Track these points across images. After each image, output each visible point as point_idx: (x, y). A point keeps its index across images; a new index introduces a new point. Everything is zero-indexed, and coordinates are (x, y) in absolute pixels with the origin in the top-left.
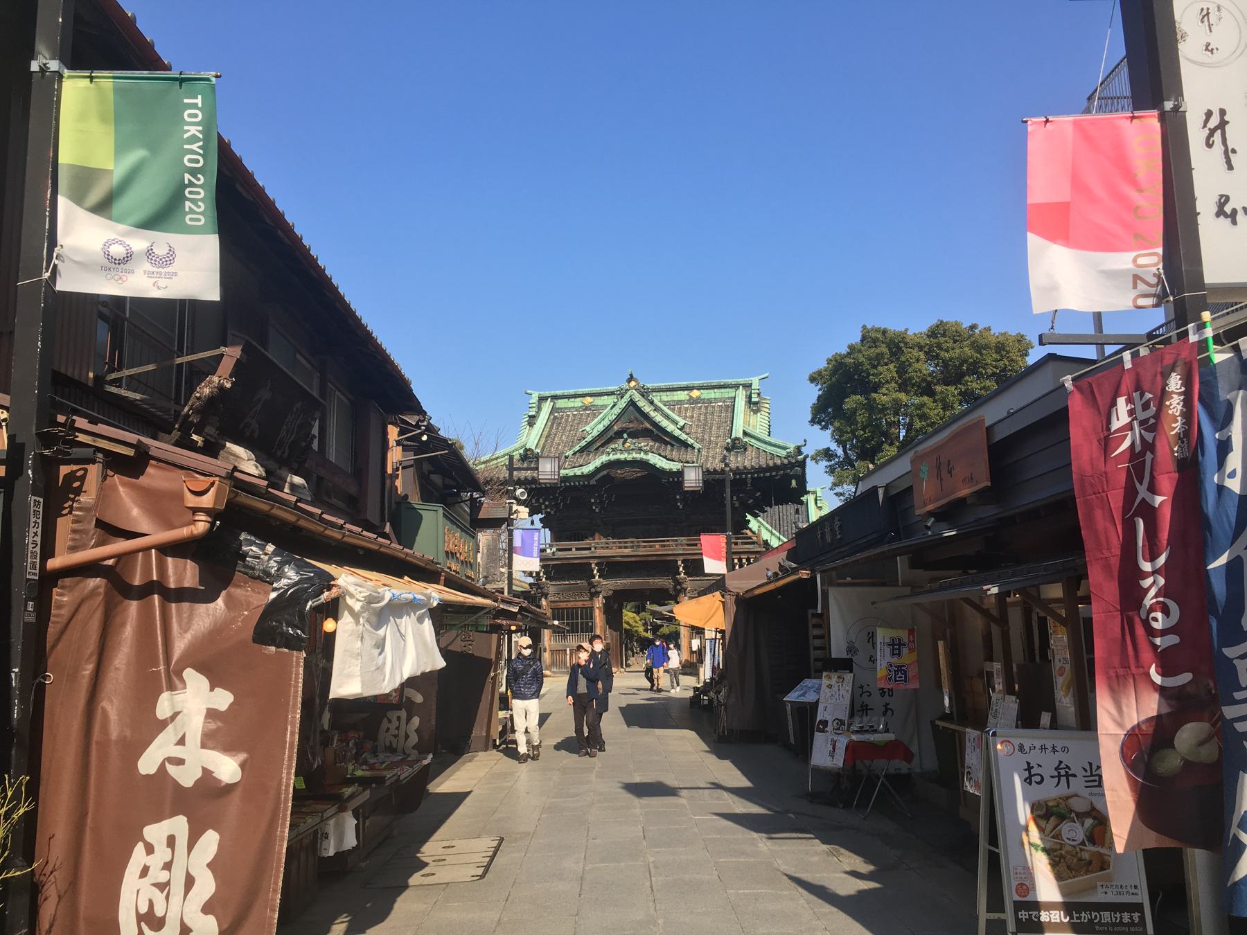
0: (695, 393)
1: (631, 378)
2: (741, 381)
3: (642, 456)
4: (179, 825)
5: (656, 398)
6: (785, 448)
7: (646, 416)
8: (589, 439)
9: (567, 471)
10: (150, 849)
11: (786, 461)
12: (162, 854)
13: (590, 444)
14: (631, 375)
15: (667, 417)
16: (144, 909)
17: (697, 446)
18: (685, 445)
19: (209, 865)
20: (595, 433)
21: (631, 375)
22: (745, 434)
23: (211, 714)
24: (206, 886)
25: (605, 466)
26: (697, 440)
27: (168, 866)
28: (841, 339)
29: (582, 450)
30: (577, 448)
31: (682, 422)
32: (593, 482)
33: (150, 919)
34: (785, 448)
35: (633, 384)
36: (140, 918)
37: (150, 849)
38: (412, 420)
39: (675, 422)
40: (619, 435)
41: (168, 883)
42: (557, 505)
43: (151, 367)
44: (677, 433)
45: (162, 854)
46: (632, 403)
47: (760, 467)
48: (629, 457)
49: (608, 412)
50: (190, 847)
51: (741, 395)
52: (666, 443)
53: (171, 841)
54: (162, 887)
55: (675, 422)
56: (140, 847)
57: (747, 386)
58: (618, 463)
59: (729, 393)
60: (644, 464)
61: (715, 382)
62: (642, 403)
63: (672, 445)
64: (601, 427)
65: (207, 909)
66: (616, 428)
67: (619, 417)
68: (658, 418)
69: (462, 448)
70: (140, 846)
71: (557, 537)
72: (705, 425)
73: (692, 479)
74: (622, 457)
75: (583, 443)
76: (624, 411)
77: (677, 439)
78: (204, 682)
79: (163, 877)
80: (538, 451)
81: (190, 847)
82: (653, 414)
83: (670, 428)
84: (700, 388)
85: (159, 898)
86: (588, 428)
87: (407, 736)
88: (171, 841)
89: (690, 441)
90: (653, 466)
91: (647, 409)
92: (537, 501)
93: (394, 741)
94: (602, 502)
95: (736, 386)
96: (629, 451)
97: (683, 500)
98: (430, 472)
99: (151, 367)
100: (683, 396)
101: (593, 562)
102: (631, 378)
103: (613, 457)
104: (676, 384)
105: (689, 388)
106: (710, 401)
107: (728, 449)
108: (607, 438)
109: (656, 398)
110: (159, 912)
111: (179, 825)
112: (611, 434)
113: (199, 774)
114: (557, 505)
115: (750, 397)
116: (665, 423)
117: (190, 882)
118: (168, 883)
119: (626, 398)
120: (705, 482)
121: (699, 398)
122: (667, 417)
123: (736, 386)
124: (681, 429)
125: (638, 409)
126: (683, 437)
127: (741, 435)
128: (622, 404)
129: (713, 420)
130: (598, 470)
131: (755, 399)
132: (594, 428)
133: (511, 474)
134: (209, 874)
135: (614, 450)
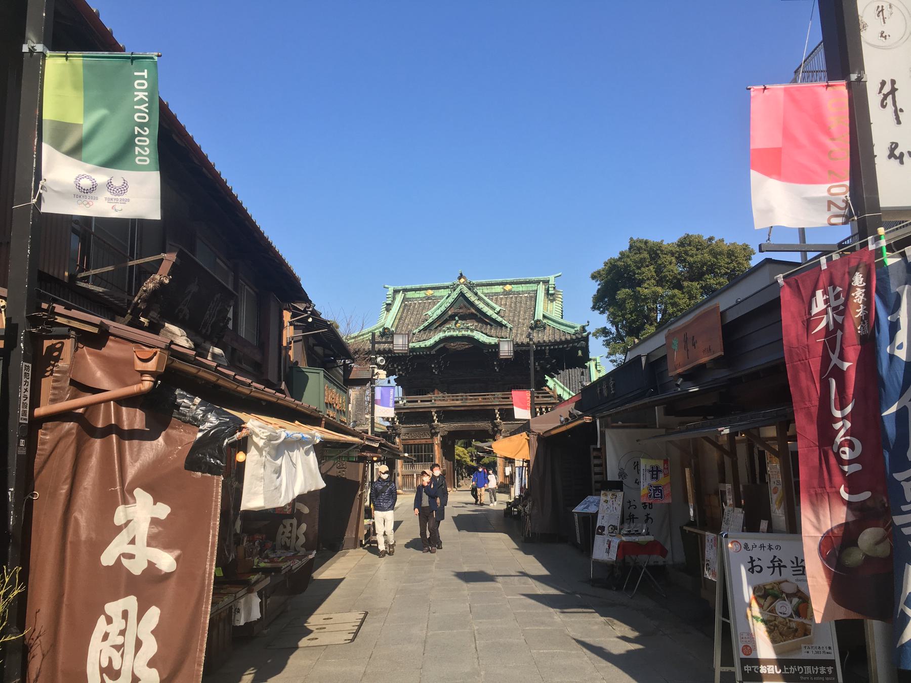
0: (508, 287)
1: (461, 276)
2: (542, 278)
3: (469, 333)
4: (131, 603)
5: (479, 291)
6: (573, 327)
7: (472, 304)
8: (430, 320)
9: (414, 344)
10: (109, 620)
11: (574, 337)
12: (119, 624)
13: (431, 324)
14: (461, 274)
15: (488, 305)
16: (105, 664)
17: (509, 326)
18: (500, 325)
19: (153, 632)
20: (435, 316)
21: (461, 274)
22: (544, 317)
23: (154, 521)
24: (151, 647)
25: (442, 340)
26: (509, 321)
27: (122, 633)
28: (614, 248)
29: (425, 329)
30: (422, 327)
31: (498, 308)
32: (433, 352)
33: (110, 671)
34: (573, 327)
35: (462, 280)
36: (102, 670)
37: (109, 620)
38: (301, 307)
39: (493, 309)
40: (452, 317)
41: (123, 645)
42: (407, 369)
44: (495, 316)
45: (119, 624)
46: (462, 294)
47: (556, 341)
48: (460, 334)
49: (444, 301)
50: (139, 619)
51: (541, 289)
52: (487, 324)
53: (125, 615)
54: (118, 648)
55: (493, 309)
56: (102, 619)
57: (546, 282)
58: (451, 339)
59: (533, 287)
60: (470, 339)
61: (522, 279)
62: (469, 295)
63: (491, 325)
64: (439, 312)
65: (151, 664)
66: (450, 313)
67: (452, 305)
68: (481, 305)
70: (102, 618)
71: (407, 392)
72: (515, 310)
73: (506, 350)
74: (455, 334)
75: (426, 324)
76: (456, 300)
77: (495, 321)
78: (149, 498)
79: (119, 640)
80: (393, 329)
81: (139, 619)
82: (477, 302)
83: (490, 312)
84: (511, 283)
85: (116, 656)
86: (429, 313)
87: (297, 538)
88: (125, 615)
89: (504, 322)
90: (477, 341)
91: (473, 298)
92: (393, 366)
93: (288, 541)
94: (440, 367)
95: (538, 282)
96: (459, 329)
97: (499, 365)
98: (314, 345)
100: (499, 289)
101: (434, 410)
102: (461, 276)
103: (447, 334)
104: (494, 280)
105: (503, 284)
106: (518, 293)
107: (532, 328)
108: (443, 320)
109: (479, 291)
110: (116, 666)
111: (131, 603)
112: (446, 317)
113: (145, 565)
114: (407, 369)
115: (548, 290)
116: (486, 309)
117: (139, 644)
118: (123, 645)
119: (458, 291)
120: (515, 352)
121: (510, 291)
122: (488, 305)
123: (538, 282)
124: (498, 313)
125: (466, 299)
126: (499, 319)
127: (541, 318)
128: (455, 295)
129: (521, 307)
130: (437, 343)
131: (551, 292)
132: (434, 313)
133: (373, 347)
134: (153, 638)
135: (448, 329)
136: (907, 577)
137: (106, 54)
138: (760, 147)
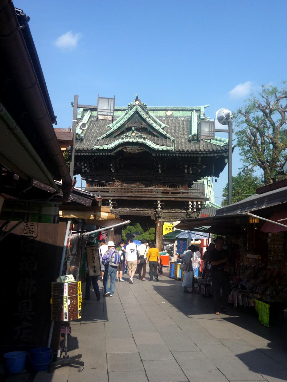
0: (169, 113)
1: (137, 99)
2: (195, 107)
3: (142, 140)
5: (151, 114)
6: (222, 141)
7: (144, 120)
8: (112, 130)
9: (99, 147)
11: (223, 149)
13: (112, 134)
14: (137, 97)
15: (156, 122)
17: (172, 138)
18: (165, 137)
20: (115, 128)
21: (137, 97)
25: (120, 145)
26: (171, 135)
29: (107, 137)
30: (104, 135)
31: (163, 125)
32: (113, 153)
34: (222, 141)
35: (137, 102)
39: (160, 125)
40: (129, 129)
43: (213, 166)
44: (161, 130)
46: (137, 112)
47: (209, 151)
48: (135, 141)
49: (122, 118)
51: (195, 116)
52: (154, 136)
55: (160, 125)
57: (198, 111)
58: (128, 144)
59: (188, 114)
61: (180, 107)
62: (142, 113)
63: (158, 137)
64: (119, 125)
66: (126, 126)
67: (129, 119)
68: (151, 122)
69: (159, 149)
72: (175, 128)
74: (131, 140)
75: (108, 133)
76: (132, 116)
77: (161, 134)
80: (83, 135)
82: (148, 119)
83: (157, 128)
84: (172, 110)
86: (111, 125)
89: (168, 135)
90: (148, 147)
91: (145, 116)
92: (80, 164)
95: (192, 110)
96: (134, 137)
99: (213, 166)
100: (162, 113)
102: (137, 99)
103: (125, 140)
104: (159, 107)
105: (166, 110)
106: (177, 117)
107: (190, 141)
108: (122, 130)
109: (151, 114)
112: (124, 129)
115: (200, 116)
116: (154, 125)
119: (134, 109)
121: (171, 115)
122: (156, 122)
123: (192, 110)
124: (163, 129)
125: (140, 116)
126: (164, 133)
128: (131, 112)
129: (179, 127)
130: (116, 147)
131: (202, 117)
132: (114, 126)
135: (126, 136)
136: (223, 314)
137: (40, 160)
138: (176, 225)
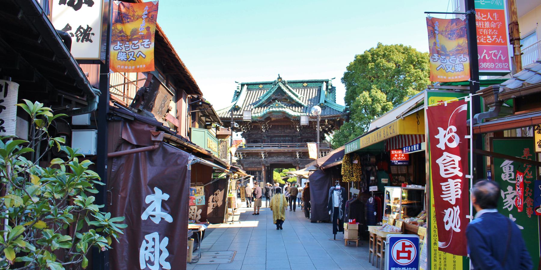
4: (156, 235)
10: (147, 242)
12: (151, 243)
16: (147, 259)
19: (166, 247)
22: (325, 102)
23: (163, 201)
24: (166, 254)
27: (153, 247)
28: (362, 48)
33: (150, 262)
36: (146, 262)
37: (147, 242)
38: (196, 96)
40: (274, 100)
41: (154, 252)
42: (248, 129)
45: (151, 243)
46: (279, 88)
50: (160, 241)
53: (154, 239)
54: (152, 253)
56: (144, 241)
60: (284, 113)
65: (167, 260)
70: (144, 241)
71: (248, 141)
73: (304, 121)
78: (160, 191)
79: (152, 250)
81: (160, 241)
85: (152, 256)
87: (197, 216)
88: (154, 239)
90: (287, 114)
93: (192, 217)
94: (266, 128)
97: (300, 128)
98: (201, 116)
101: (262, 152)
110: (152, 260)
111: (156, 235)
113: (160, 220)
114: (248, 129)
117: (161, 252)
118: (154, 252)
120: (310, 122)
125: (282, 90)
127: (324, 102)
133: (232, 117)
134: (166, 249)
